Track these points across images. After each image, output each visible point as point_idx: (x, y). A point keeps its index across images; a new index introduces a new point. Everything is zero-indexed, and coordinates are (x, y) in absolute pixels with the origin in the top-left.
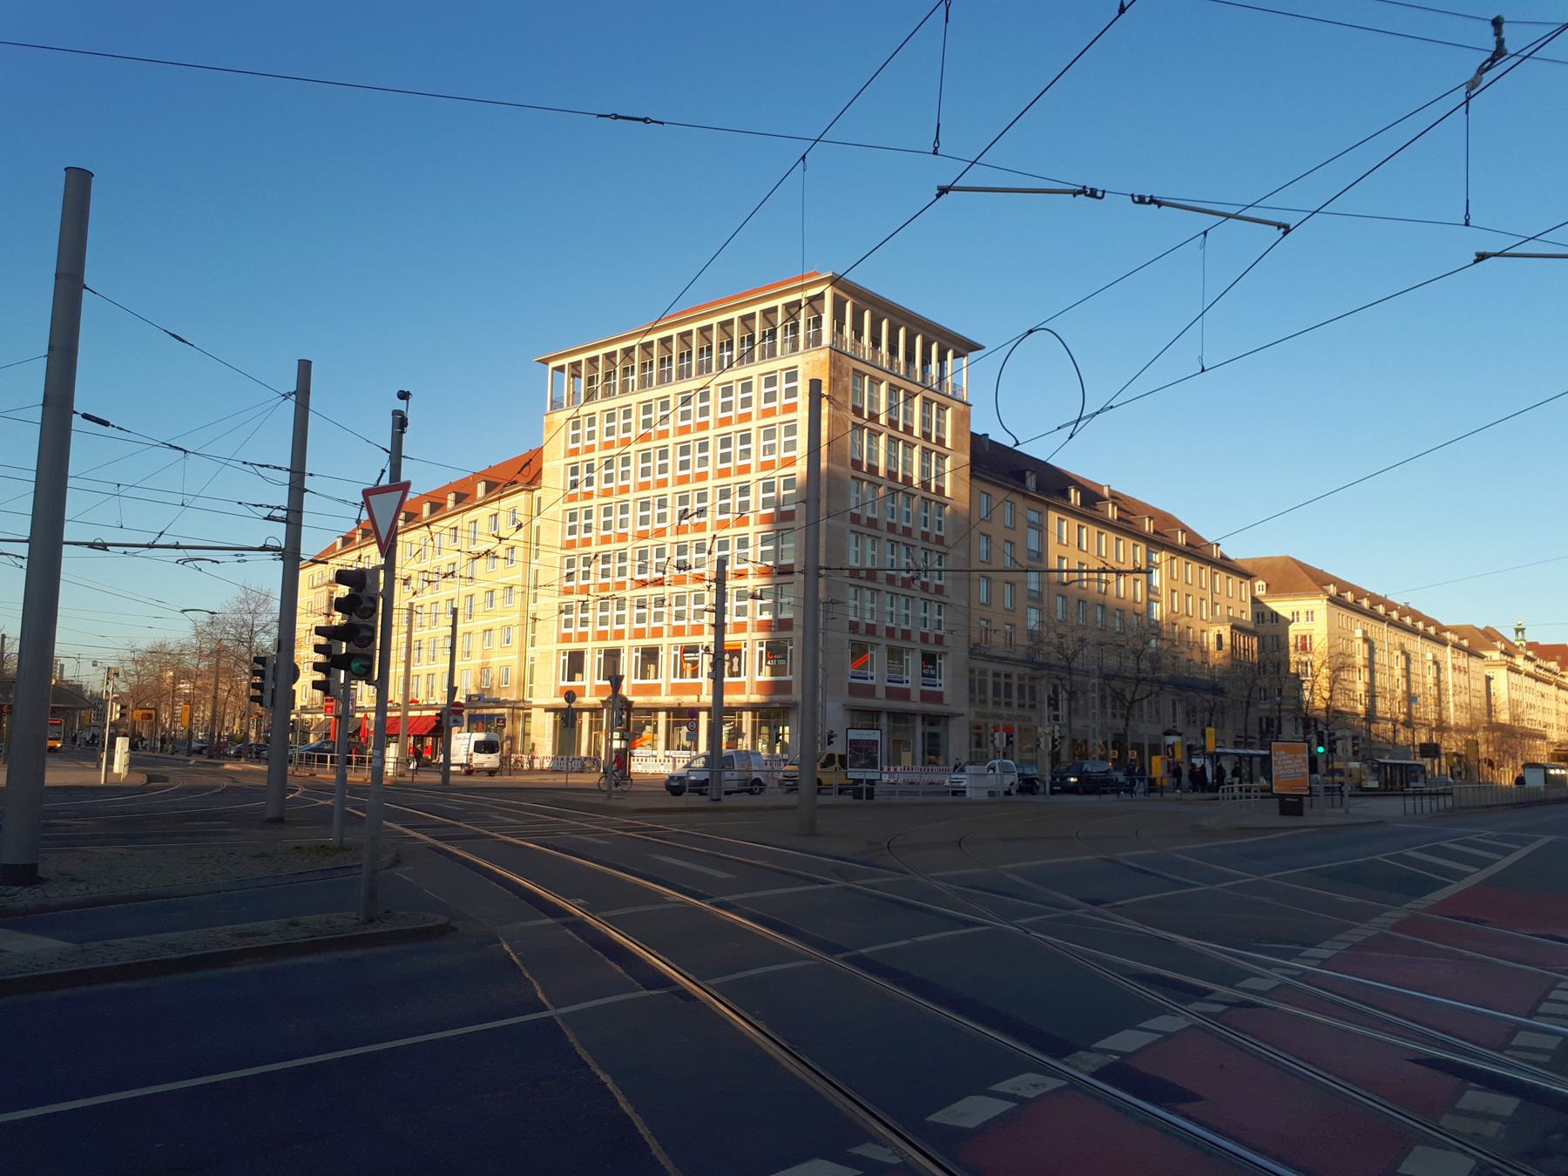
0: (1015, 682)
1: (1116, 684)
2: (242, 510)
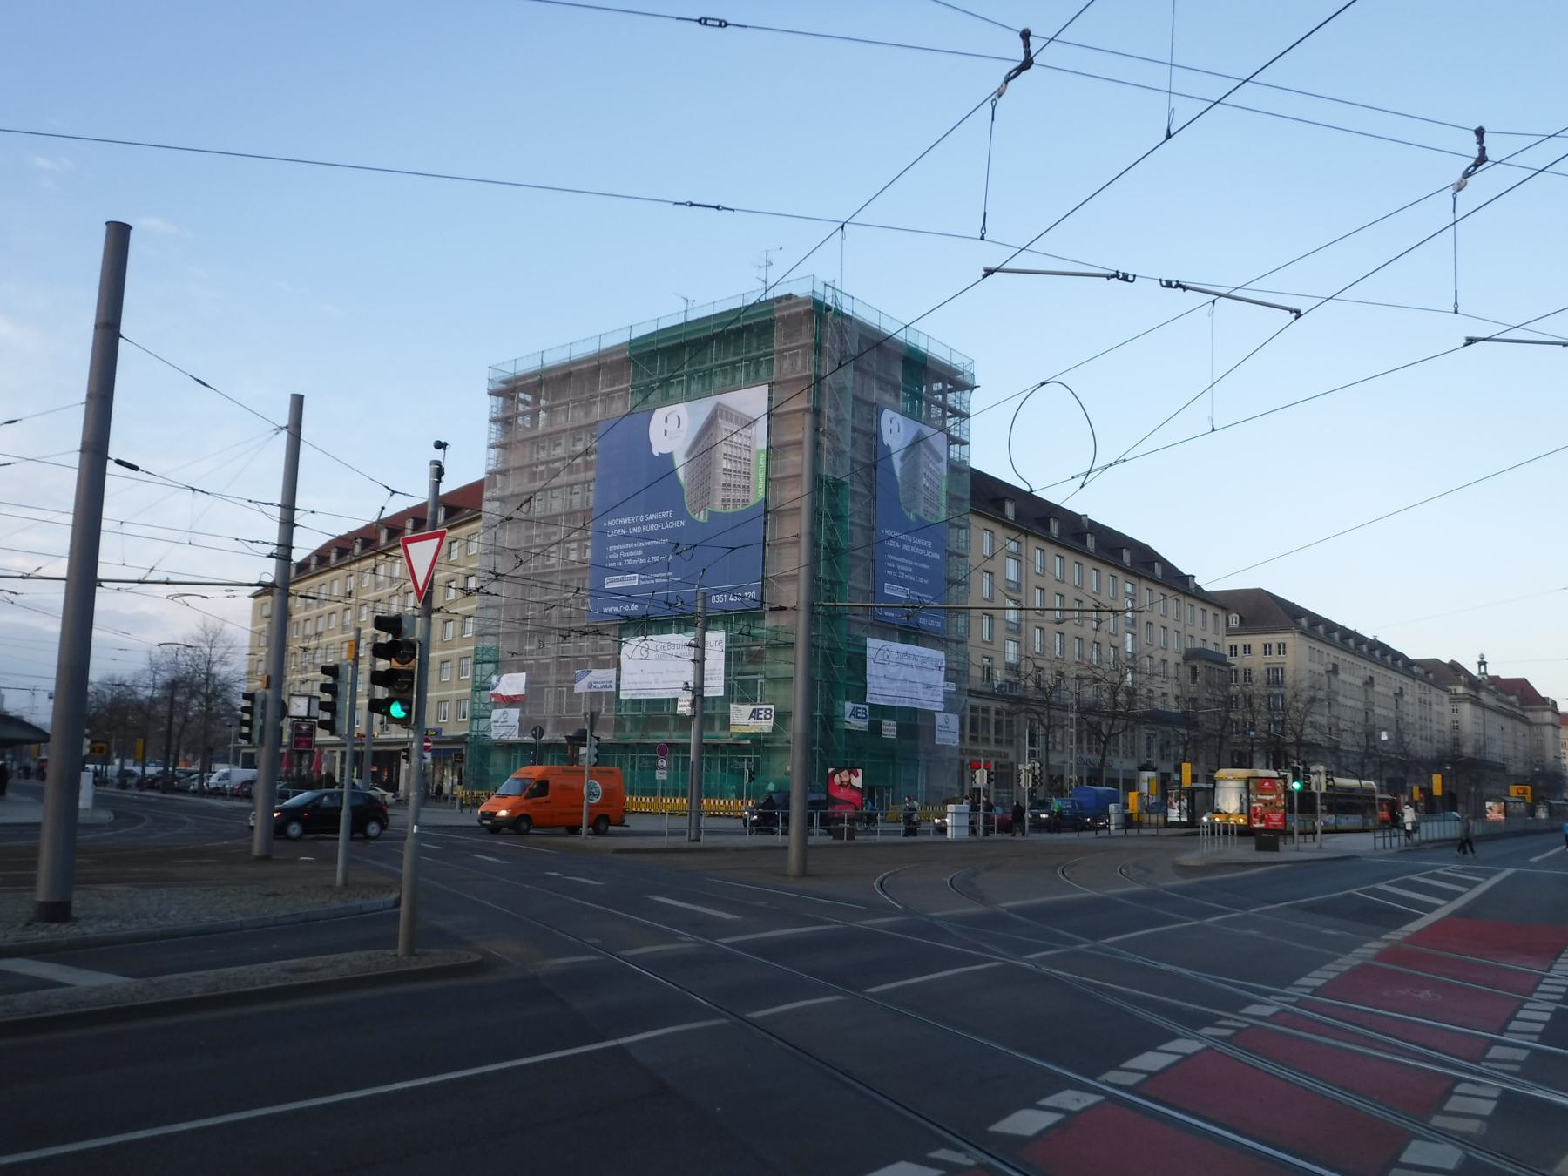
0: (993, 715)
1: (1093, 719)
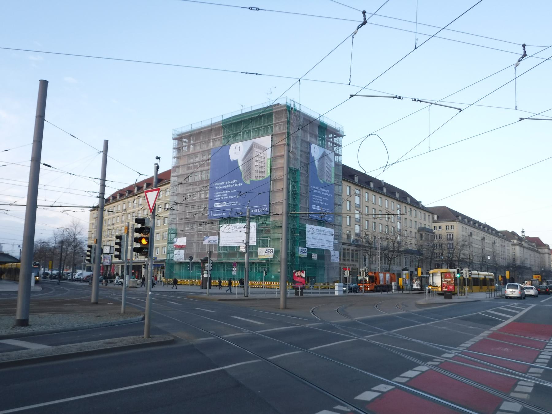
1: (386, 252)
2: (86, 194)
